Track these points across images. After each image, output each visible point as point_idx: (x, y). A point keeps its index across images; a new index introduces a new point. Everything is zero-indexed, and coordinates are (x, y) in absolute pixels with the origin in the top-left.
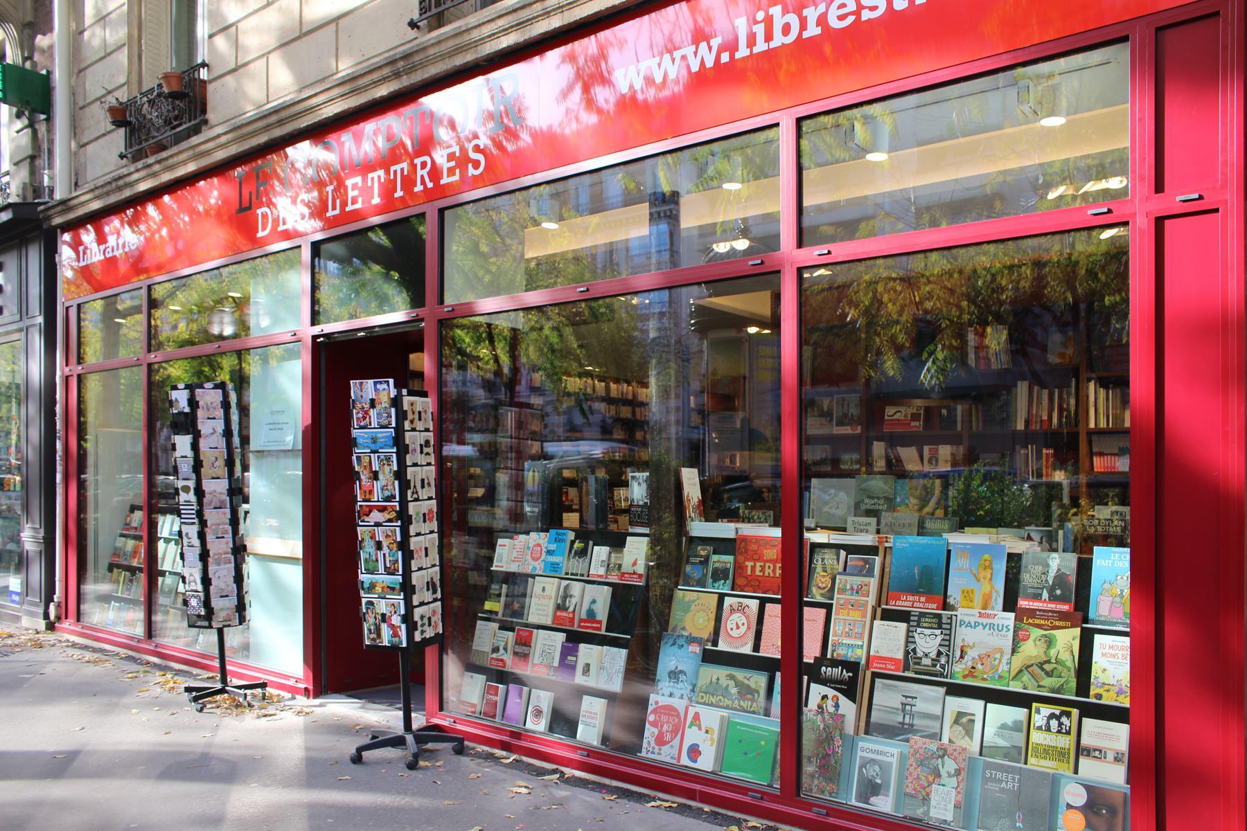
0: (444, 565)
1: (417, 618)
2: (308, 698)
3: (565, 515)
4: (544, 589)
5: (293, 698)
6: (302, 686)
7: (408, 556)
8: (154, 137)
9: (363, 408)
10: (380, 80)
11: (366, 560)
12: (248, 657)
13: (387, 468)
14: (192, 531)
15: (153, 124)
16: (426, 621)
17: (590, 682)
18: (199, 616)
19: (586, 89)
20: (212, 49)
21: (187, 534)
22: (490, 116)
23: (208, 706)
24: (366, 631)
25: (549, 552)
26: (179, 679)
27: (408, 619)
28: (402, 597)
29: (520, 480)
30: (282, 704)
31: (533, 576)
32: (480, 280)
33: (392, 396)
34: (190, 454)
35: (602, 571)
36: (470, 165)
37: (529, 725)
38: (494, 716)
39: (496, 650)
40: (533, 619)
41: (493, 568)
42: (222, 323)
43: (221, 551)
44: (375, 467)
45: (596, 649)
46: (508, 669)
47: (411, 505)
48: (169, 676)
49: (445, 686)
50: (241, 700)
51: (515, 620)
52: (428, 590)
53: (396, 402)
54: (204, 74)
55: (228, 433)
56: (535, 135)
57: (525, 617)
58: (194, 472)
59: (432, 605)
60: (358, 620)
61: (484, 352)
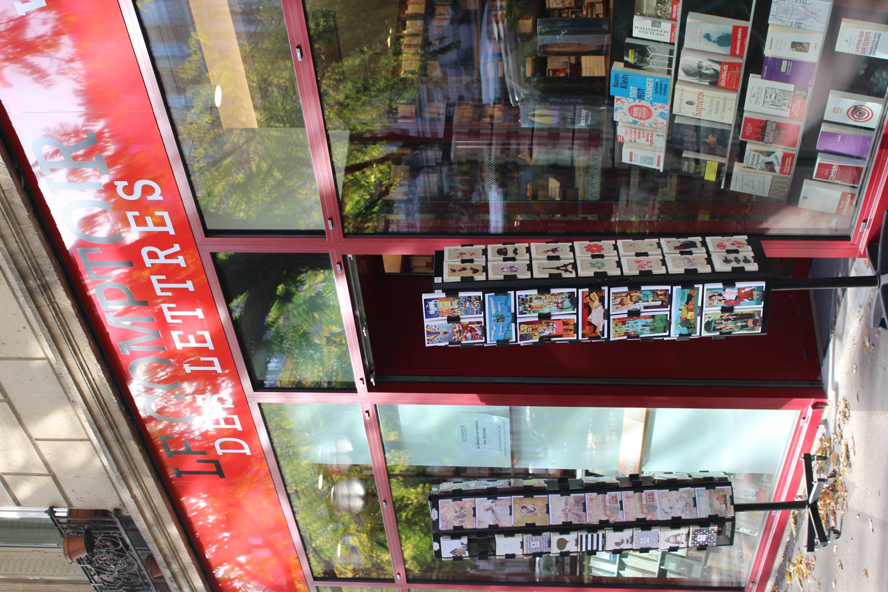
0: (658, 233)
1: (727, 268)
2: (826, 404)
3: (585, 73)
4: (690, 103)
5: (825, 422)
6: (810, 411)
7: (647, 278)
8: (140, 570)
9: (459, 331)
10: (54, 308)
11: (652, 330)
12: (770, 476)
13: (535, 303)
14: (613, 538)
15: (125, 570)
16: (731, 256)
17: (816, 40)
18: (719, 533)
19: (31, 47)
20: (32, 501)
21: (617, 544)
22: (74, 172)
23: (832, 524)
24: (745, 332)
25: (641, 96)
26: (795, 558)
27: (728, 279)
28: (701, 286)
29: (546, 134)
30: (832, 436)
31: (672, 117)
32: (279, 185)
33: (444, 295)
34: (518, 538)
35: (666, 26)
36: (149, 198)
37: (873, 123)
38: (859, 170)
39: (770, 166)
40: (729, 117)
41: (661, 169)
42: (349, 497)
43: (638, 505)
44: (533, 317)
45: (772, 33)
46: (795, 151)
47: (581, 273)
48: (791, 569)
49: (812, 233)
50: (826, 485)
51: (730, 141)
52: (691, 253)
53: (451, 291)
54: (62, 512)
55: (492, 494)
56: (92, 116)
57: (726, 128)
58: (540, 534)
59: (711, 249)
60: (729, 342)
61: (373, 176)
